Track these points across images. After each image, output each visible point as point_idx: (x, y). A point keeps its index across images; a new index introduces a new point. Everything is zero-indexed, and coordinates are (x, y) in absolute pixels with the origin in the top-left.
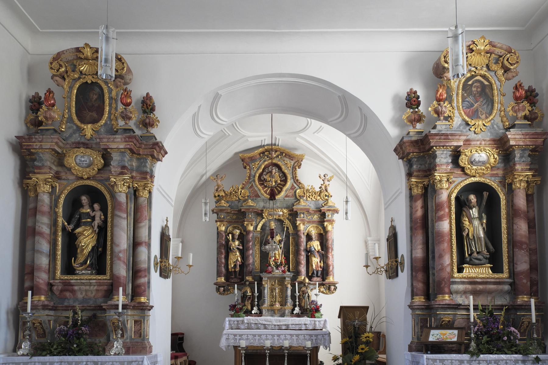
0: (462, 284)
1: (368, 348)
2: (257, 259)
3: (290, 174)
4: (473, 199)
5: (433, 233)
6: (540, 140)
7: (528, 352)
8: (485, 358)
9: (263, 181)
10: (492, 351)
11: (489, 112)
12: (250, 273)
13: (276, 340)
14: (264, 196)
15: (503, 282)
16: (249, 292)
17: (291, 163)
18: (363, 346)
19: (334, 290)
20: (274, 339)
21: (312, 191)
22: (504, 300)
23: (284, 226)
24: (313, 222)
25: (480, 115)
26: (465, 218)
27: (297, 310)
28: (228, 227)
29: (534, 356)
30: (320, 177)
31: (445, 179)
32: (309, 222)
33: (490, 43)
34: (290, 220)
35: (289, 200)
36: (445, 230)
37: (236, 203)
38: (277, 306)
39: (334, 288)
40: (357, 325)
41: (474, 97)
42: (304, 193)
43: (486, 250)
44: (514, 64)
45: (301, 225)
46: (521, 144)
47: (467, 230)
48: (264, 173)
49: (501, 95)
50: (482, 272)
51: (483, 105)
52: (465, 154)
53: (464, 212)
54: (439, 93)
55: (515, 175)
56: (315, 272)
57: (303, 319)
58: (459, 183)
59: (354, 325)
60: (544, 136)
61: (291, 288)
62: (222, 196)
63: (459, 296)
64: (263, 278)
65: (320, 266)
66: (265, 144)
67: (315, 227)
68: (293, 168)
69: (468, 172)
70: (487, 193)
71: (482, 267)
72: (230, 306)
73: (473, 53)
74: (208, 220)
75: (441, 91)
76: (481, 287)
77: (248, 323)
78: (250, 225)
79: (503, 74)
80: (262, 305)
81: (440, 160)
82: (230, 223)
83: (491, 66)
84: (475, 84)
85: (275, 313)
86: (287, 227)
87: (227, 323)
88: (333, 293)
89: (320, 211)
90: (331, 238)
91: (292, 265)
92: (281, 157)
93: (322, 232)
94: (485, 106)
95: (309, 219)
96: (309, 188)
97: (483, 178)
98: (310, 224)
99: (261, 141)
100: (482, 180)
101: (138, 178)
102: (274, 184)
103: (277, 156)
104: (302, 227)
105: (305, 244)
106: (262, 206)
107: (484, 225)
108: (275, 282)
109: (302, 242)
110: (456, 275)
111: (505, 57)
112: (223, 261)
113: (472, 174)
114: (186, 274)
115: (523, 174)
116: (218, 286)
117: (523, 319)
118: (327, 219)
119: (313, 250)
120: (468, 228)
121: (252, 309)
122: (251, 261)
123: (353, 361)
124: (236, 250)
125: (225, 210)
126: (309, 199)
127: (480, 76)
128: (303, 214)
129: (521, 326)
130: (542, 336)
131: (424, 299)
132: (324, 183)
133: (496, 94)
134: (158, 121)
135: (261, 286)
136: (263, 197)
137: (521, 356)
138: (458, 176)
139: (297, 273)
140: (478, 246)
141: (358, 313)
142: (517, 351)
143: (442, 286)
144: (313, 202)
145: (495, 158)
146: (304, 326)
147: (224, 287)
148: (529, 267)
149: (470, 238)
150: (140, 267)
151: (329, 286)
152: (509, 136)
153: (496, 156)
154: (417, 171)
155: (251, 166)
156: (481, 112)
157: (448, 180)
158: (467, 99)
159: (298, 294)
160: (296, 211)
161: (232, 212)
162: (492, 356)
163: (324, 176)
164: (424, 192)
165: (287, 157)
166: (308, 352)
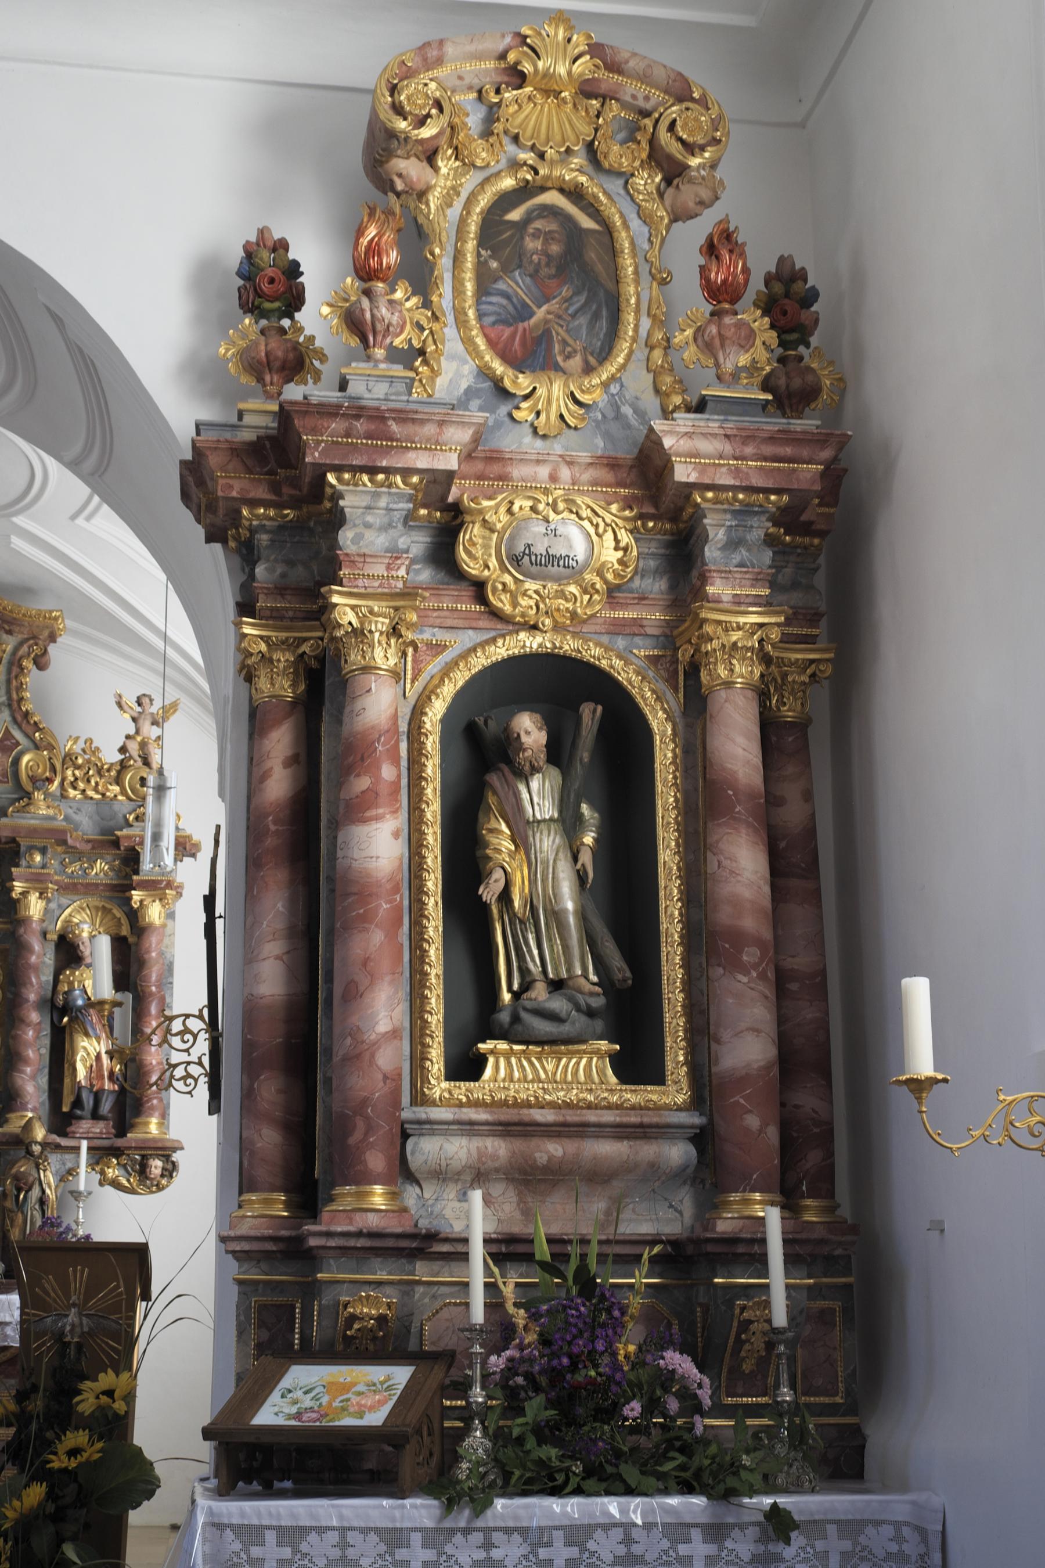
0: (462, 1133)
1: (99, 1445)
4: (528, 733)
5: (331, 879)
6: (809, 470)
7: (731, 1482)
8: (516, 1518)
10: (560, 1478)
11: (602, 349)
15: (657, 1126)
19: (162, 1176)
21: (89, 761)
22: (671, 1214)
24: (89, 889)
25: (559, 359)
26: (493, 819)
29: (768, 1501)
30: (119, 705)
31: (382, 624)
32: (72, 888)
33: (595, 50)
36: (372, 865)
39: (163, 1169)
40: (72, 1331)
41: (531, 276)
43: (597, 972)
44: (702, 148)
45: (33, 898)
46: (721, 482)
47: (498, 874)
49: (653, 277)
50: (569, 1078)
51: (574, 316)
52: (484, 521)
53: (490, 794)
54: (364, 241)
55: (705, 621)
56: (88, 1101)
58: (465, 655)
60: (822, 449)
63: (451, 1192)
65: (111, 1074)
67: (97, 908)
68: (11, 664)
69: (502, 603)
70: (595, 711)
71: (578, 1052)
73: (528, 90)
75: (372, 232)
76: (554, 1149)
79: (658, 189)
81: (358, 538)
83: (603, 148)
84: (538, 224)
88: (160, 1188)
89: (116, 843)
90: (161, 954)
93: (125, 931)
94: (583, 320)
95: (71, 876)
96: (77, 748)
97: (575, 635)
98: (75, 898)
100: (569, 645)
104: (35, 907)
105: (47, 977)
107: (586, 858)
109: (36, 969)
110: (439, 1087)
111: (661, 115)
113: (523, 615)
115: (742, 620)
117: (743, 1308)
120: (503, 868)
123: (10, 1514)
126: (72, 793)
127: (562, 190)
128: (43, 851)
129: (739, 1343)
130: (848, 1393)
131: (288, 1205)
132: (137, 732)
133: (630, 270)
137: (698, 1501)
138: (460, 623)
140: (552, 951)
141: (80, 1275)
142: (686, 1475)
143: (351, 1141)
144: (89, 808)
145: (622, 544)
148: (772, 1052)
149: (515, 915)
151: (143, 1157)
152: (668, 442)
153: (625, 538)
154: (269, 593)
156: (564, 343)
157: (394, 631)
158: (501, 286)
160: (13, 840)
162: (556, 1505)
163: (140, 704)
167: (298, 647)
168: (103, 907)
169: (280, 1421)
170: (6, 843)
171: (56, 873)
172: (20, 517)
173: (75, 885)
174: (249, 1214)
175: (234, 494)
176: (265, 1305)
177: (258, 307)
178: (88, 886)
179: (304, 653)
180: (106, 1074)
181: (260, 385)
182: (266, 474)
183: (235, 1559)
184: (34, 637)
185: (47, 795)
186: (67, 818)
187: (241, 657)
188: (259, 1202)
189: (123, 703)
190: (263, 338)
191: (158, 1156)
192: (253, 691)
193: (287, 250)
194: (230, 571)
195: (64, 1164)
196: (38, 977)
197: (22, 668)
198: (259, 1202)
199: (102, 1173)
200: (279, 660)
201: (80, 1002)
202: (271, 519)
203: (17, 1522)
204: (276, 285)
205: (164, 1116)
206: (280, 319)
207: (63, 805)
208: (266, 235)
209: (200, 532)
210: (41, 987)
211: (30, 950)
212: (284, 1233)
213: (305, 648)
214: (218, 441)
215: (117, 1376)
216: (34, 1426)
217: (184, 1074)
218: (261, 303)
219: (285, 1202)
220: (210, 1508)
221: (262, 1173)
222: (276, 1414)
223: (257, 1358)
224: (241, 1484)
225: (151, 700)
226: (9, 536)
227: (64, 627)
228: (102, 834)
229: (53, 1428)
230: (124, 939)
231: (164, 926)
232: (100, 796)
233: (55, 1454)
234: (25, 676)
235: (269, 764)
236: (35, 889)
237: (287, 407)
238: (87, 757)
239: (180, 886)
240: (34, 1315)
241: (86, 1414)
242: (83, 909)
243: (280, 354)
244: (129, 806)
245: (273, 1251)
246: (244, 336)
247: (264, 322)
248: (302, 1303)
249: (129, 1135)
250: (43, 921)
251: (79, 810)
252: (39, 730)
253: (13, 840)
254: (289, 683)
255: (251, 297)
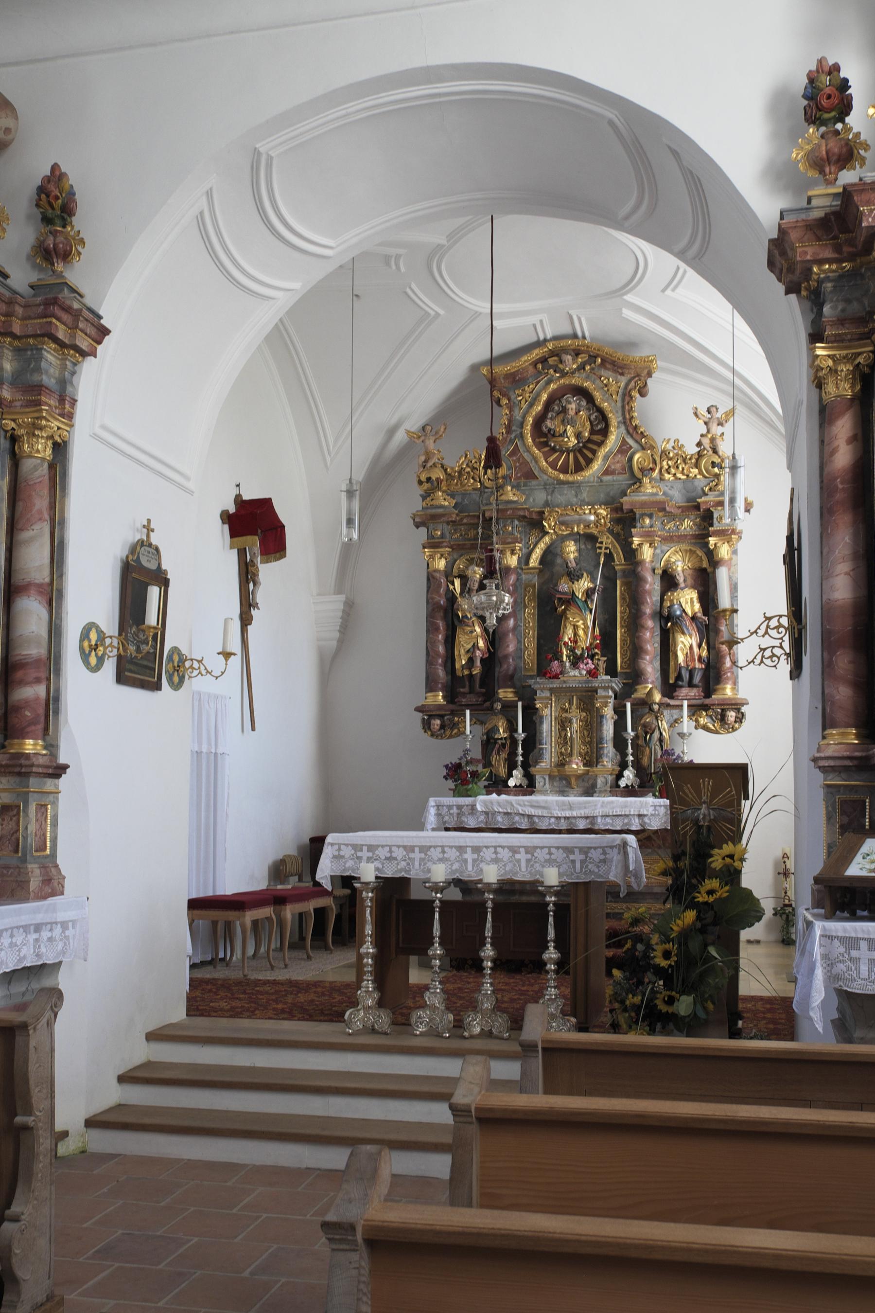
1: (727, 888)
2: (529, 641)
3: (617, 412)
9: (545, 435)
12: (510, 680)
13: (470, 861)
14: (546, 474)
16: (501, 731)
17: (616, 382)
18: (714, 884)
19: (735, 722)
20: (465, 861)
21: (677, 454)
23: (598, 551)
24: (681, 538)
27: (629, 776)
28: (455, 561)
30: (696, 414)
32: (669, 539)
34: (616, 536)
35: (614, 481)
37: (475, 496)
38: (574, 766)
39: (736, 717)
40: (704, 818)
42: (655, 462)
45: (646, 547)
48: (550, 415)
56: (686, 675)
57: (635, 802)
59: (696, 821)
61: (616, 717)
62: (438, 479)
64: (538, 692)
65: (700, 658)
66: (549, 337)
67: (686, 551)
68: (624, 395)
72: (446, 766)
74: (355, 536)
77: (486, 813)
78: (509, 553)
80: (537, 763)
82: (459, 549)
85: (569, 785)
86: (605, 554)
87: (432, 811)
88: (734, 729)
89: (697, 507)
91: (621, 657)
92: (592, 369)
93: (705, 564)
96: (669, 446)
98: (672, 545)
99: (533, 329)
101: (18, 404)
102: (574, 441)
103: (582, 367)
104: (647, 553)
105: (656, 597)
106: (543, 502)
108: (571, 703)
109: (649, 593)
112: (441, 649)
114: (217, 678)
116: (428, 714)
118: (717, 526)
119: (678, 613)
121: (510, 775)
122: (511, 648)
123: (675, 928)
124: (474, 619)
125: (443, 515)
126: (667, 476)
128: (651, 516)
131: (857, 736)
132: (708, 431)
134: (82, 242)
135: (535, 713)
136: (545, 477)
139: (635, 677)
141: (707, 785)
144: (679, 485)
146: (637, 820)
147: (441, 717)
150: (20, 654)
151: (723, 710)
154: (833, 324)
155: (513, 397)
159: (632, 734)
160: (631, 511)
161: (465, 521)
163: (709, 412)
164: (862, 390)
165: (608, 366)
166: (548, 899)
167: (855, 359)
168: (690, 550)
169: (864, 873)
170: (627, 513)
171: (659, 530)
172: (629, 295)
173: (671, 537)
174: (832, 742)
175: (809, 257)
176: (845, 801)
177: (819, 118)
178: (679, 537)
179: (860, 363)
180: (696, 658)
181: (821, 176)
182: (831, 239)
183: (841, 958)
184: (638, 375)
185: (651, 479)
186: (665, 494)
187: (812, 372)
188: (839, 734)
189: (698, 413)
190: (824, 141)
191: (732, 709)
192: (823, 394)
193: (839, 71)
194: (802, 312)
195: (672, 716)
196: (651, 598)
197: (631, 397)
198: (839, 734)
199: (697, 721)
200: (842, 370)
201: (678, 613)
202: (834, 271)
203: (680, 933)
204: (832, 99)
205: (735, 683)
206: (835, 124)
207: (662, 485)
208: (824, 63)
209: (781, 288)
210: (653, 604)
211: (645, 581)
212: (857, 754)
213: (861, 359)
214: (797, 221)
215: (735, 845)
216: (685, 876)
217: (771, 654)
218: (821, 115)
219: (855, 734)
220: (824, 926)
221: (840, 716)
222: (861, 869)
223: (842, 834)
224: (838, 912)
225: (717, 409)
226: (621, 309)
227: (657, 366)
228: (688, 502)
229: (696, 877)
230: (705, 570)
231: (731, 559)
232: (685, 477)
233: (699, 893)
234: (634, 402)
235: (836, 444)
236: (647, 541)
237: (849, 189)
238: (676, 452)
239: (740, 532)
240: (681, 809)
241: (717, 869)
242: (677, 552)
243: (836, 150)
244: (704, 482)
245: (850, 766)
246: (809, 142)
247: (823, 129)
248: (870, 800)
249: (713, 696)
250: (653, 562)
251: (672, 487)
252: (644, 437)
253: (631, 511)
254: (849, 386)
255: (814, 112)
